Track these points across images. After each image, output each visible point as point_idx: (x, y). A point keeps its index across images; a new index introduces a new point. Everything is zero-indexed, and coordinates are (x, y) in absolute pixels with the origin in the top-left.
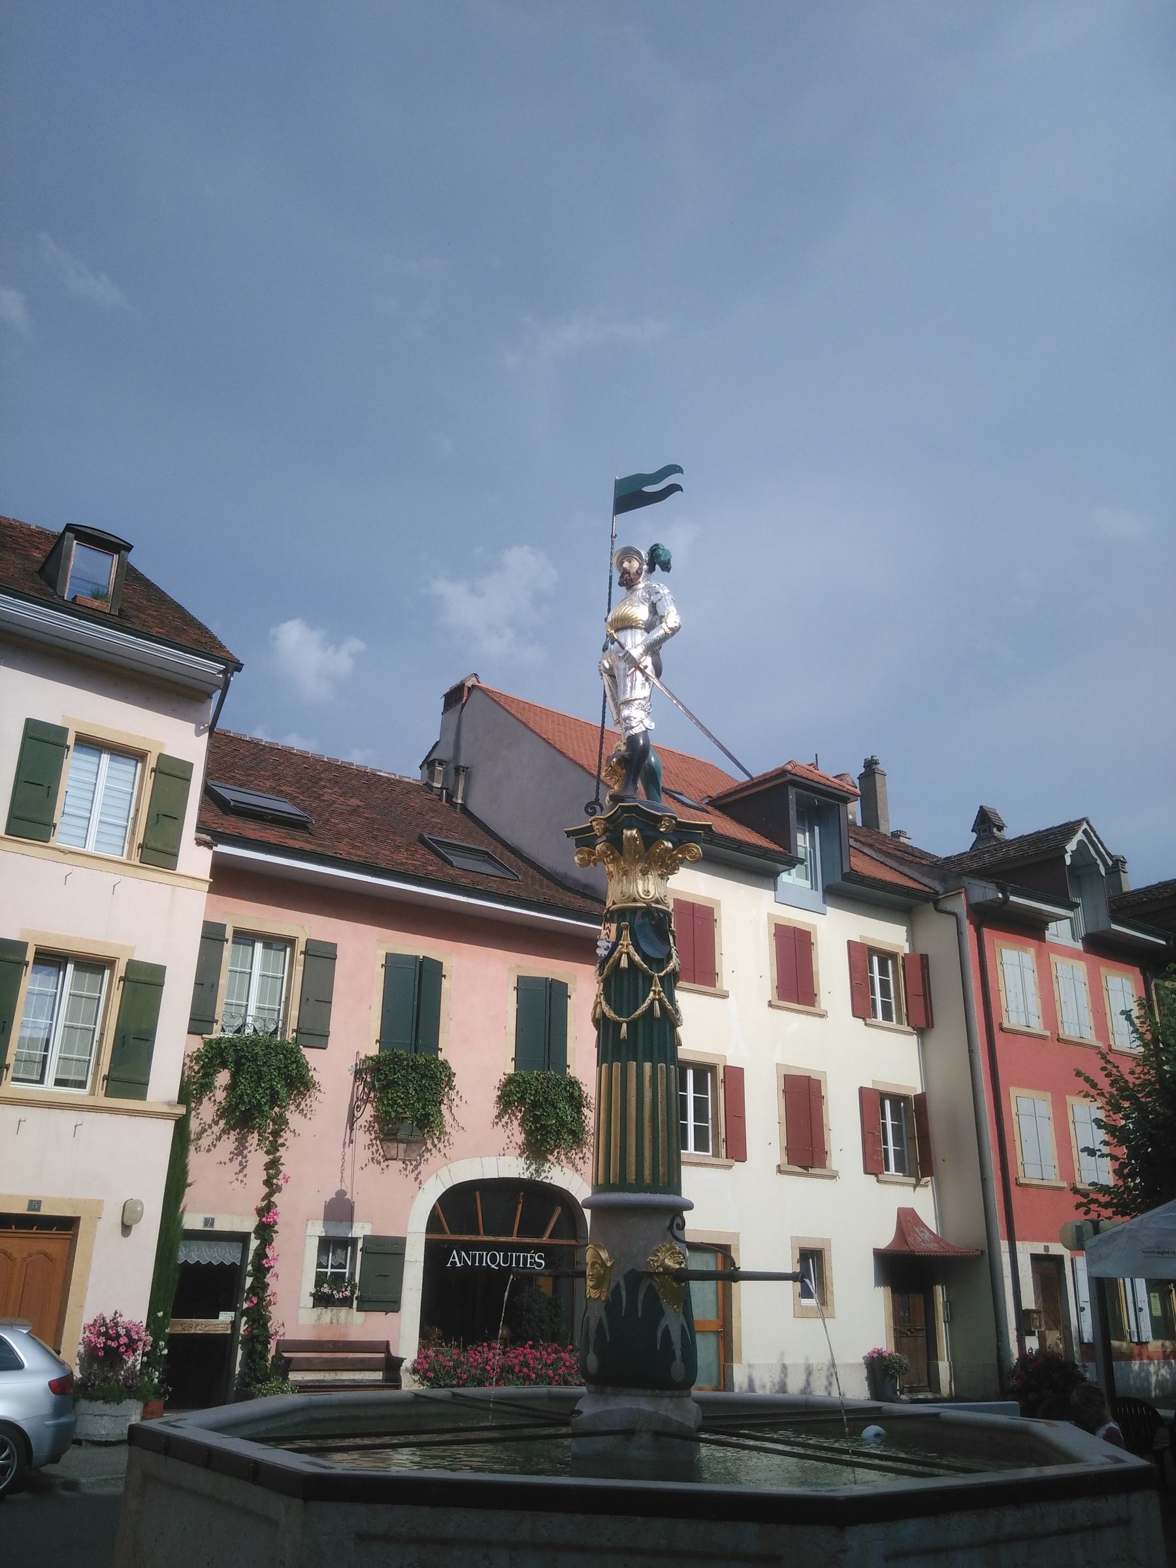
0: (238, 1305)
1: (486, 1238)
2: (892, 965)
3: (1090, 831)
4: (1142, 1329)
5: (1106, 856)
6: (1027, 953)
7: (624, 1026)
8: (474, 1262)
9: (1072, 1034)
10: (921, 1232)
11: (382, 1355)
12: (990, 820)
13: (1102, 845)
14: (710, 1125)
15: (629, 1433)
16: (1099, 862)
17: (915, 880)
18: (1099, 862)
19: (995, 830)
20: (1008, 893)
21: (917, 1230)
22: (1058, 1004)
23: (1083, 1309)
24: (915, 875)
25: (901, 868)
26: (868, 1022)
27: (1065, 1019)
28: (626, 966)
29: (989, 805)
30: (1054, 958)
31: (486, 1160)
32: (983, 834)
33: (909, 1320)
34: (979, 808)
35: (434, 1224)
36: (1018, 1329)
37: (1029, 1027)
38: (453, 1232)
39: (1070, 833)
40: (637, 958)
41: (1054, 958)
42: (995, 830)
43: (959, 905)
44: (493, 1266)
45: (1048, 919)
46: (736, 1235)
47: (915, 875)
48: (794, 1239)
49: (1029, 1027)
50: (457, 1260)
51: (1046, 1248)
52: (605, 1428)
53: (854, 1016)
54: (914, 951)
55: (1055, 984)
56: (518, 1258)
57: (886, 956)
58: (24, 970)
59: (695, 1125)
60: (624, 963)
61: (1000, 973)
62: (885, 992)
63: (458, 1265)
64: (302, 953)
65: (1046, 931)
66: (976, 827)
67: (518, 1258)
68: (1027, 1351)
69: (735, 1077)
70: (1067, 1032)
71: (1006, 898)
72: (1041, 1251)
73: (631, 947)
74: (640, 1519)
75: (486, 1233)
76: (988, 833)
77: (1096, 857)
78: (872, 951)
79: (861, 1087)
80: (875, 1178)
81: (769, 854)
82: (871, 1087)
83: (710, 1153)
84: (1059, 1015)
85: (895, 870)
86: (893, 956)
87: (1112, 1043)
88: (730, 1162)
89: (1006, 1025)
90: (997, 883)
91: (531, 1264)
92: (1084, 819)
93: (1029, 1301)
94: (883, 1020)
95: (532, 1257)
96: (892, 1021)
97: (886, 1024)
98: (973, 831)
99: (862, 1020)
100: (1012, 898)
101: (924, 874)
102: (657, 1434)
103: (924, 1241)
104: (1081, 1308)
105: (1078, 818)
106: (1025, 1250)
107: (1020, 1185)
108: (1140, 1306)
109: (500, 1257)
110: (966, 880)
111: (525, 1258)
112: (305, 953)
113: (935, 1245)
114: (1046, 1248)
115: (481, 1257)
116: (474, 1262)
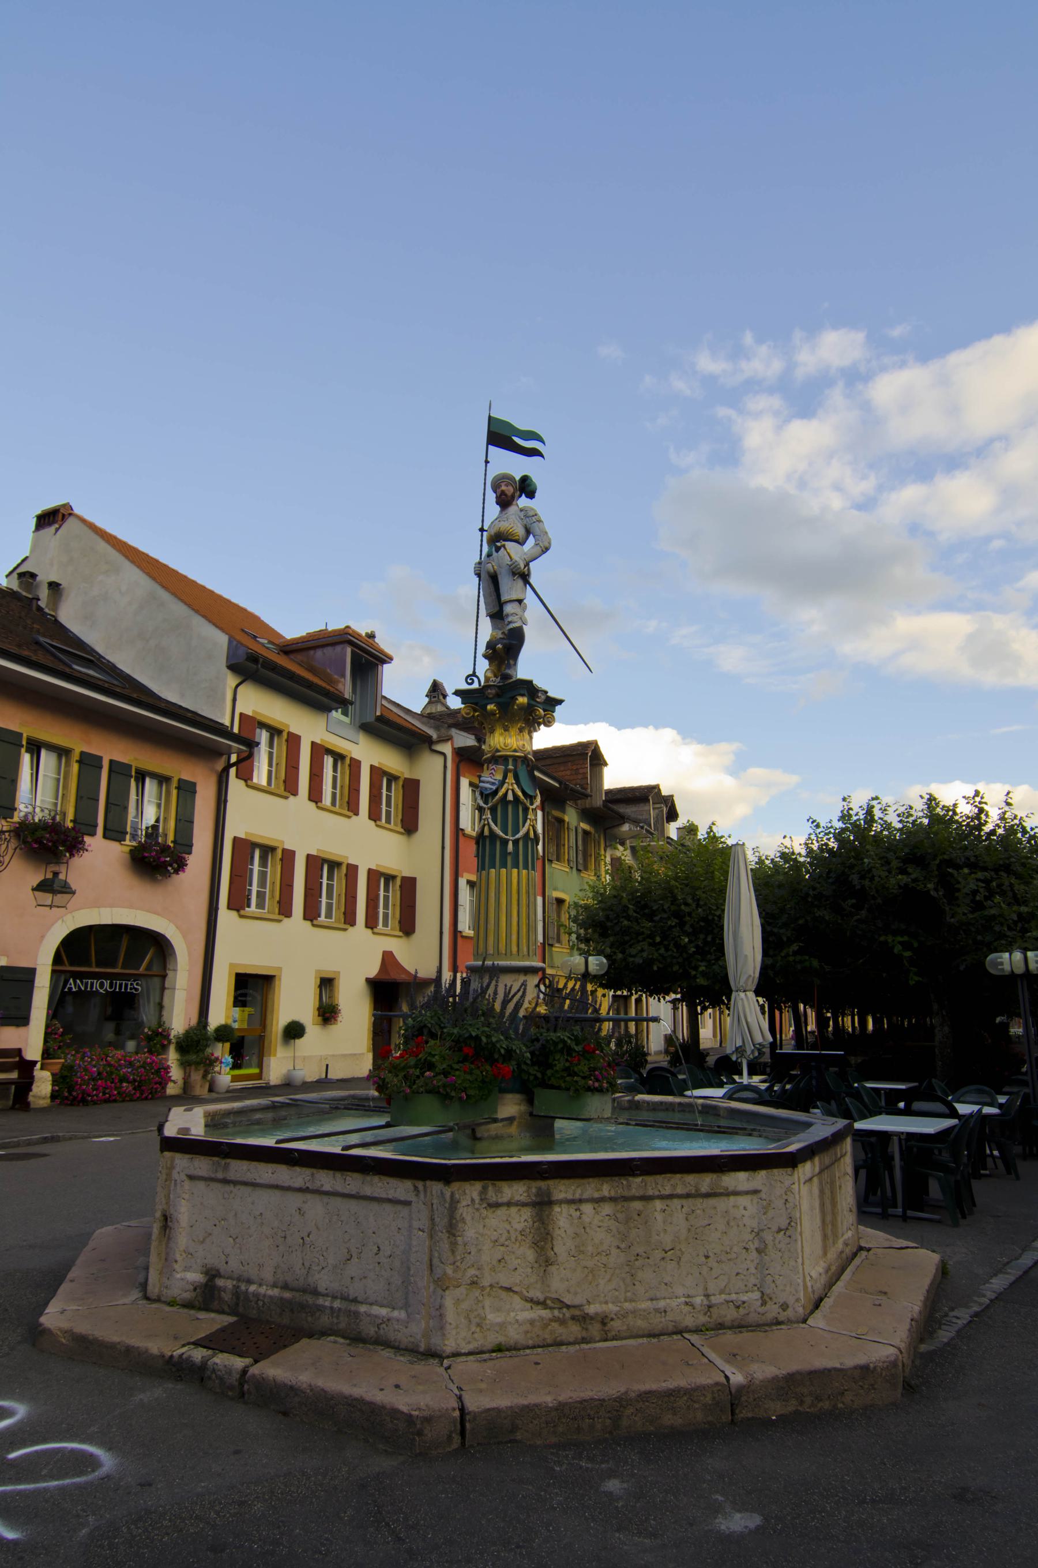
0: (774, 1418)
1: (97, 970)
8: (86, 987)
11: (17, 1059)
14: (267, 891)
29: (440, 679)
31: (102, 910)
35: (57, 959)
38: (71, 964)
40: (520, 794)
43: (447, 748)
44: (101, 991)
46: (280, 969)
48: (318, 971)
50: (73, 986)
56: (121, 985)
57: (392, 778)
58: (133, 796)
60: (510, 797)
62: (388, 805)
63: (74, 990)
64: (77, 761)
67: (121, 985)
68: (251, 991)
69: (356, 867)
73: (515, 786)
75: (97, 966)
78: (385, 773)
86: (396, 778)
88: (281, 917)
91: (131, 989)
95: (131, 984)
97: (387, 826)
98: (427, 696)
107: (463, 937)
109: (107, 984)
111: (126, 985)
112: (80, 762)
115: (92, 984)
116: (86, 987)
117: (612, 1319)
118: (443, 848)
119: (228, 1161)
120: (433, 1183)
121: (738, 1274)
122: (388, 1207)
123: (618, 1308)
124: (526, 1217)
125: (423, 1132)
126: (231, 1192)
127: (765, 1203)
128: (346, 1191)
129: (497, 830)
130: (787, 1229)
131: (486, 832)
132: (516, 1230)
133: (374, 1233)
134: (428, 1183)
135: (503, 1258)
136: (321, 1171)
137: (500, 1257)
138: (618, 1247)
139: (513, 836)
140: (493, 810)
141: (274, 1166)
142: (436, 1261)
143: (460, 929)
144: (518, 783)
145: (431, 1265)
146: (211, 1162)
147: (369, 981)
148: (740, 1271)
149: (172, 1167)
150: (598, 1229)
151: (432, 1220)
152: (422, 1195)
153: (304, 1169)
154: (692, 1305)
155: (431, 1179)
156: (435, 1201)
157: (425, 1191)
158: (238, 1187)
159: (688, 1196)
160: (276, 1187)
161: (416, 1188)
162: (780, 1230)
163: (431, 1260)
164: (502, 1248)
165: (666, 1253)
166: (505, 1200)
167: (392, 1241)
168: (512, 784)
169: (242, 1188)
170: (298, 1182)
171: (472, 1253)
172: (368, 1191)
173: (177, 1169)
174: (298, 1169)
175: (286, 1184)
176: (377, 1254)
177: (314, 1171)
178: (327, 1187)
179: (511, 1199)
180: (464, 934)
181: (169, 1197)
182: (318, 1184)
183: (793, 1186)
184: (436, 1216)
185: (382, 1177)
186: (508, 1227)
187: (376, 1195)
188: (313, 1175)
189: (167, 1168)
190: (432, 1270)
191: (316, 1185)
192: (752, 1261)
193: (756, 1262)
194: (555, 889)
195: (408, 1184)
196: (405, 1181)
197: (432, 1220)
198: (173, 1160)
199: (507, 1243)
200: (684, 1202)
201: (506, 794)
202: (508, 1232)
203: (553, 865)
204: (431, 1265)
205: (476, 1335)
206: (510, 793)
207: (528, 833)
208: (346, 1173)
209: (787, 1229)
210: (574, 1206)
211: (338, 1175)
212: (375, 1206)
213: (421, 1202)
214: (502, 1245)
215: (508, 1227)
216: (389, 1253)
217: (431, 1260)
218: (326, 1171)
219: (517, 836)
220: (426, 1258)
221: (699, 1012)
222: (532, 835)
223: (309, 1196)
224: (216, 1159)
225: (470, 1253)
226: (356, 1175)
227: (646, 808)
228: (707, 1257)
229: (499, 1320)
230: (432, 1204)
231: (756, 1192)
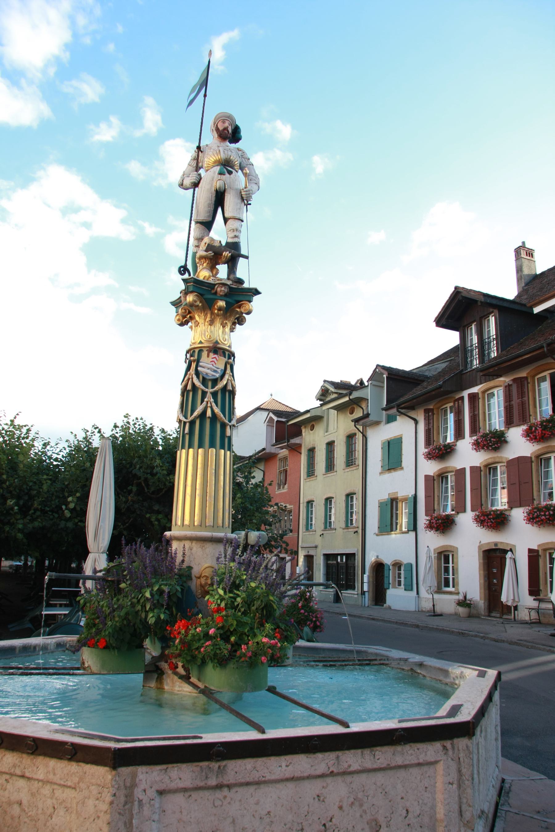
98: (341, 381)
119: (224, 763)
120: (459, 739)
122: (415, 771)
126: (225, 797)
128: (375, 766)
131: (189, 387)
133: (402, 798)
134: (456, 740)
136: (347, 752)
139: (213, 387)
141: (289, 758)
142: (464, 807)
145: (461, 811)
146: (199, 769)
149: (134, 785)
151: (459, 771)
152: (450, 752)
153: (327, 754)
155: (458, 737)
156: (461, 755)
157: (453, 748)
158: (233, 790)
160: (292, 779)
161: (444, 747)
163: (460, 807)
167: (421, 801)
169: (241, 790)
170: (321, 769)
172: (399, 760)
173: (142, 786)
174: (320, 755)
175: (306, 774)
176: (406, 817)
177: (340, 753)
178: (355, 767)
181: (131, 823)
182: (346, 765)
184: (463, 768)
185: (412, 744)
187: (407, 762)
188: (338, 757)
189: (126, 787)
190: (461, 816)
191: (344, 766)
195: (438, 745)
196: (434, 743)
197: (459, 771)
198: (134, 776)
204: (461, 811)
207: (226, 385)
208: (375, 749)
211: (367, 752)
212: (402, 773)
213: (450, 759)
216: (418, 812)
217: (460, 807)
218: (352, 751)
219: (216, 388)
220: (456, 807)
222: (230, 388)
223: (329, 780)
224: (205, 764)
226: (386, 749)
230: (459, 759)
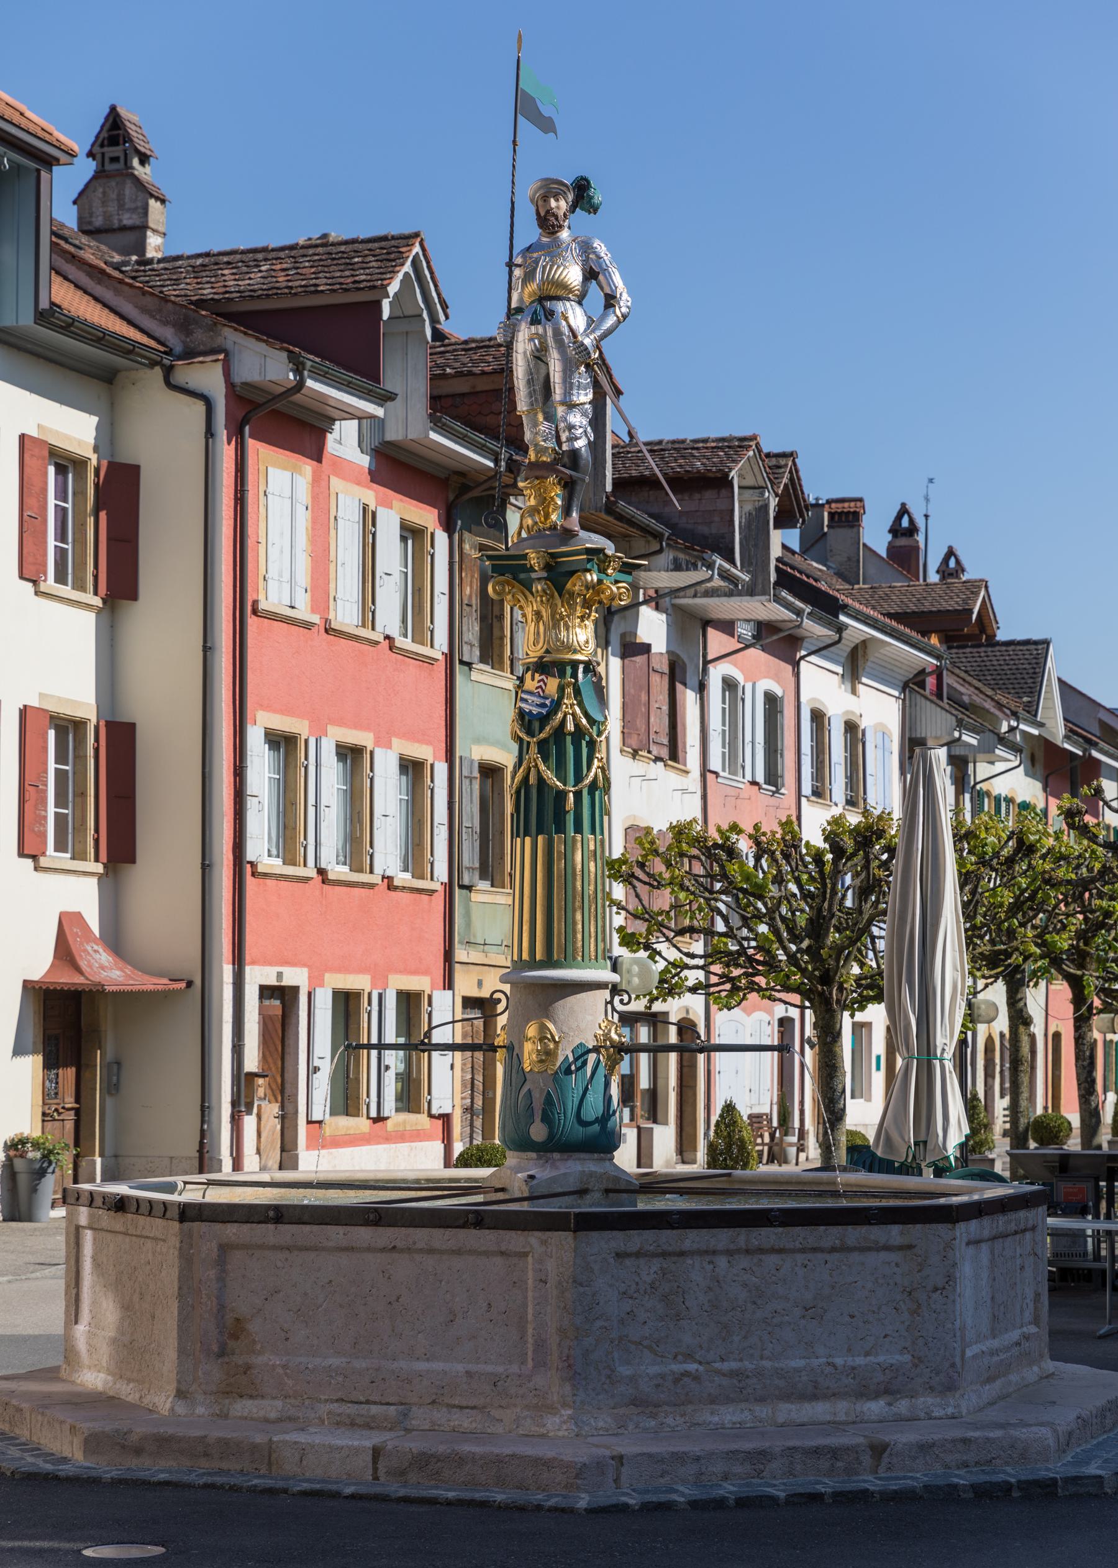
2: (74, 480)
3: (422, 258)
4: (386, 1098)
5: (438, 306)
6: (301, 475)
7: (571, 795)
9: (347, 621)
10: (96, 951)
12: (128, 138)
13: (436, 286)
15: (582, 1192)
16: (425, 315)
17: (122, 317)
18: (425, 315)
19: (136, 162)
20: (306, 373)
21: (89, 949)
22: (332, 567)
23: (316, 1070)
24: (128, 309)
25: (99, 290)
26: (42, 589)
27: (339, 596)
28: (573, 729)
30: (336, 483)
32: (109, 167)
33: (56, 1094)
34: (108, 110)
36: (235, 1104)
37: (293, 607)
39: (394, 260)
41: (336, 483)
42: (136, 162)
45: (334, 413)
47: (128, 309)
49: (293, 607)
51: (280, 975)
52: (560, 1190)
53: (22, 577)
54: (112, 456)
55: (332, 532)
59: (55, 812)
60: (570, 726)
61: (262, 510)
65: (329, 435)
66: (97, 149)
70: (339, 618)
71: (300, 385)
72: (272, 981)
74: (822, 1228)
76: (120, 165)
77: (422, 306)
79: (25, 706)
80: (32, 864)
81: (77, 328)
82: (37, 706)
83: (68, 855)
84: (332, 586)
85: (86, 292)
87: (331, 616)
89: (263, 605)
90: (290, 352)
92: (417, 235)
93: (252, 1063)
94: (56, 581)
96: (67, 585)
97: (66, 591)
99: (31, 584)
100: (310, 383)
101: (144, 310)
102: (607, 1191)
103: (103, 968)
104: (315, 1067)
105: (407, 231)
106: (257, 976)
108: (315, 1065)
110: (230, 336)
113: (118, 973)
114: (280, 975)
117: (748, 1377)
118: (207, 649)
121: (885, 1336)
123: (754, 1366)
124: (655, 1269)
125: (501, 1198)
127: (920, 1259)
129: (549, 775)
130: (944, 1288)
132: (645, 1282)
135: (632, 1311)
137: (629, 1310)
138: (755, 1303)
140: (542, 746)
143: (250, 855)
144: (581, 704)
147: (28, 987)
148: (889, 1333)
150: (733, 1284)
154: (834, 1366)
159: (833, 1250)
162: (936, 1289)
164: (630, 1301)
165: (807, 1310)
166: (635, 1249)
168: (572, 705)
171: (601, 1304)
179: (641, 1249)
180: (260, 869)
183: (953, 1242)
186: (637, 1279)
192: (903, 1322)
193: (907, 1323)
194: (478, 740)
199: (635, 1295)
200: (827, 1256)
201: (563, 722)
202: (637, 1284)
203: (475, 675)
205: (605, 1386)
206: (569, 718)
209: (944, 1288)
210: (708, 1258)
214: (631, 1298)
215: (637, 1279)
221: (778, 1131)
225: (598, 1304)
227: (721, 505)
228: (852, 1317)
229: (628, 1373)
231: (910, 1247)
